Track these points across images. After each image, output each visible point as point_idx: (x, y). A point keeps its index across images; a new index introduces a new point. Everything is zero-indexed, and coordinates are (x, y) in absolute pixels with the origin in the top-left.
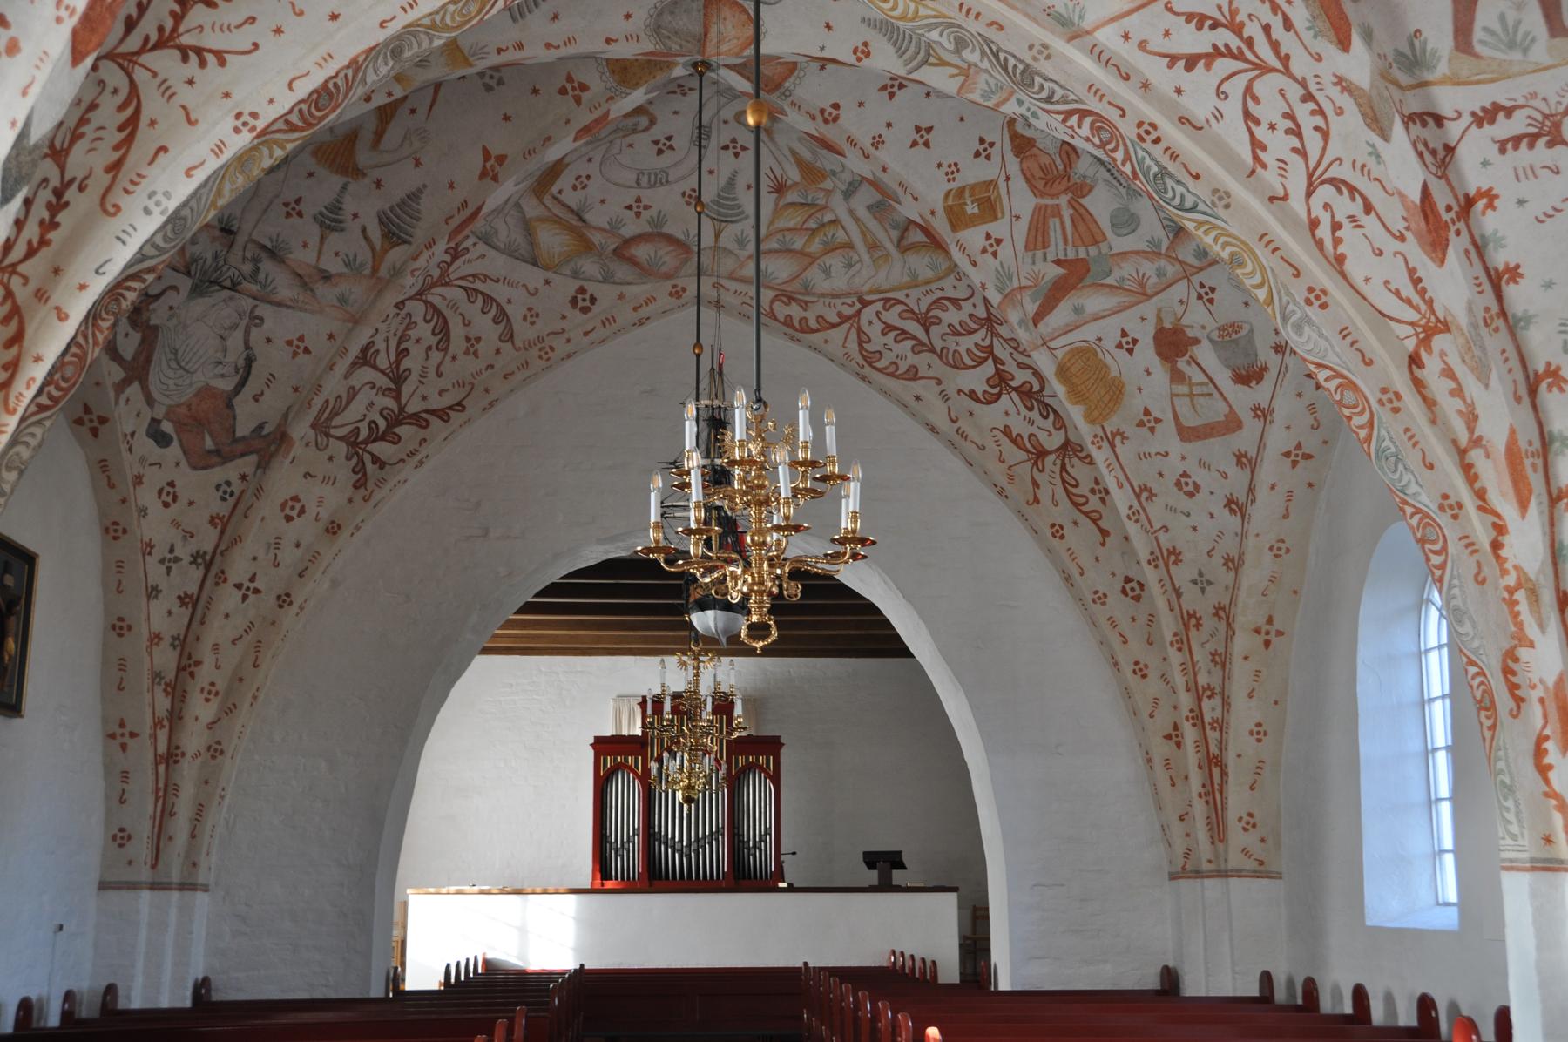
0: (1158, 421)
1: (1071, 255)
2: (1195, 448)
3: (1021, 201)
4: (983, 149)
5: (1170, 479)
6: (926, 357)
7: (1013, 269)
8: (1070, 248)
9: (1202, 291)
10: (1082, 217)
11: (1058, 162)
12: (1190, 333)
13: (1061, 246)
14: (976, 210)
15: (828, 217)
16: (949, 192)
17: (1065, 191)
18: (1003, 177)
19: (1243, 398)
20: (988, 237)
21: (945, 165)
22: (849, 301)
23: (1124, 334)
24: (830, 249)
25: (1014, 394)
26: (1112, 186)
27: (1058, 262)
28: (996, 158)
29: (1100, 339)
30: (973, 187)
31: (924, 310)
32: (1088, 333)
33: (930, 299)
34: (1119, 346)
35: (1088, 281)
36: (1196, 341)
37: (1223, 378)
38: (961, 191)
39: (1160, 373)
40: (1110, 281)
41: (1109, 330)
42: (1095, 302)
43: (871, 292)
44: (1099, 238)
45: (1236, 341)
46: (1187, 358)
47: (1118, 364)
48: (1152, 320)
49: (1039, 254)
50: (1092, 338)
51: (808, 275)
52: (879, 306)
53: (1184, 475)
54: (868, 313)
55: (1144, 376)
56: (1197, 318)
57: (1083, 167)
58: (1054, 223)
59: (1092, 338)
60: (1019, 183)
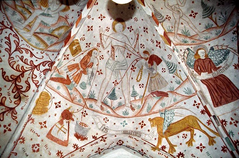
0: (45, 127)
1: (70, 78)
2: (48, 141)
3: (78, 59)
4: (88, 45)
5: (32, 143)
6: (7, 54)
7: (62, 66)
8: (72, 77)
9: (84, 113)
10: (79, 76)
11: (89, 64)
12: (73, 117)
13: (71, 75)
14: (74, 49)
15: (31, 11)
16: (78, 40)
17: (83, 69)
18: (82, 52)
19: (73, 140)
20: (68, 55)
21: (84, 37)
22: (9, 24)
23: (59, 103)
24: (21, 13)
25: (14, 85)
26: (88, 78)
27: (68, 76)
28: (87, 49)
29: (54, 98)
30: (79, 46)
31: (21, 47)
32: (53, 94)
33: (26, 47)
34: (56, 104)
35: (66, 86)
36: (73, 120)
37: (72, 132)
38: (78, 43)
39: (58, 118)
40: (70, 91)
41: (58, 99)
42: (62, 90)
43: (15, 30)
44: (77, 82)
45: (83, 128)
46: (67, 121)
47: (51, 106)
48: (68, 107)
49: (68, 70)
50: (53, 96)
51: (10, 8)
52: (13, 33)
53: (38, 145)
54: (9, 31)
55: (53, 116)
56: (77, 116)
57: (90, 70)
58: (76, 70)
59: (53, 96)
60: (82, 57)
